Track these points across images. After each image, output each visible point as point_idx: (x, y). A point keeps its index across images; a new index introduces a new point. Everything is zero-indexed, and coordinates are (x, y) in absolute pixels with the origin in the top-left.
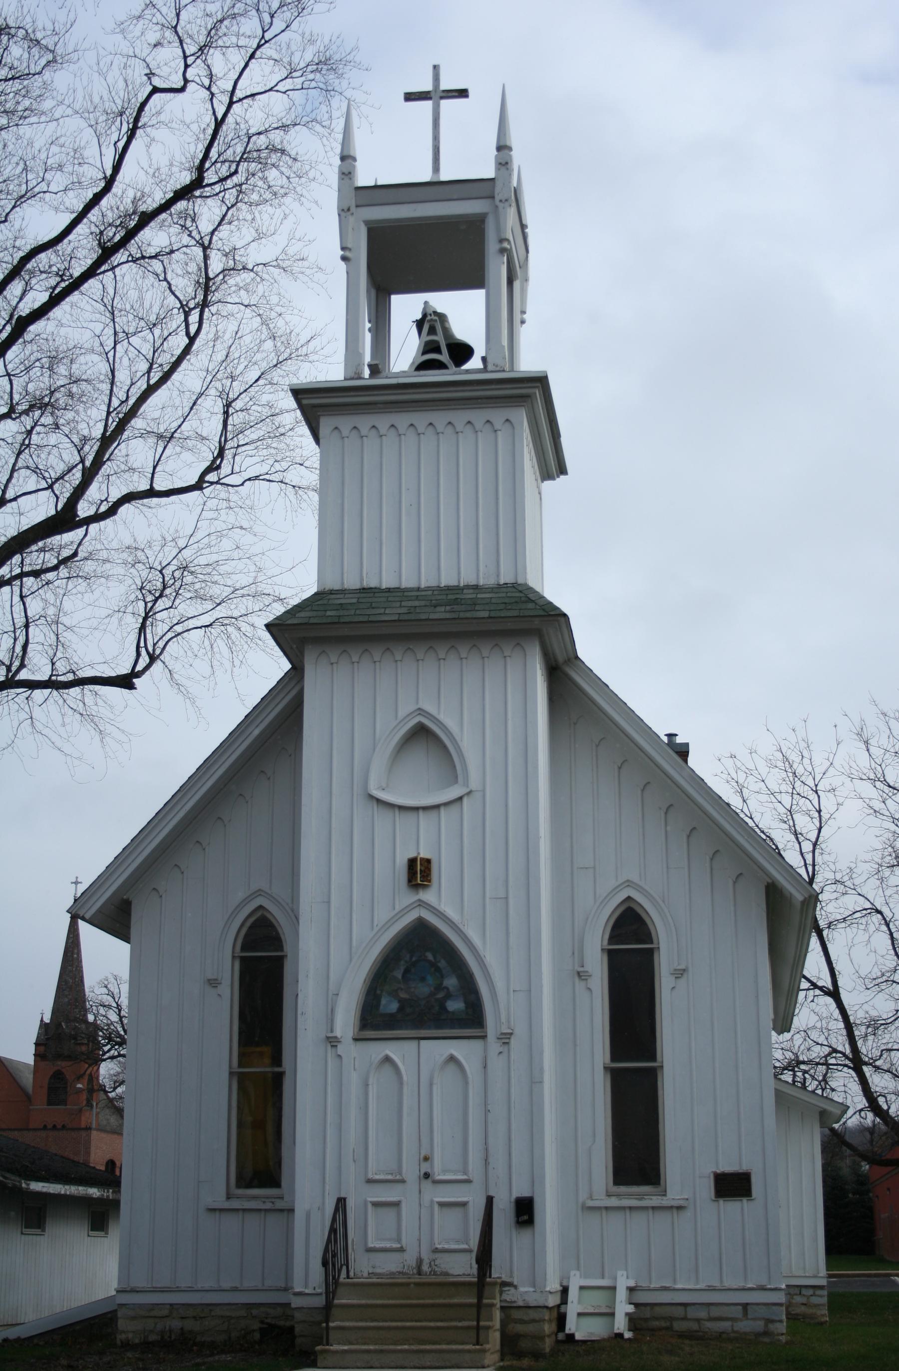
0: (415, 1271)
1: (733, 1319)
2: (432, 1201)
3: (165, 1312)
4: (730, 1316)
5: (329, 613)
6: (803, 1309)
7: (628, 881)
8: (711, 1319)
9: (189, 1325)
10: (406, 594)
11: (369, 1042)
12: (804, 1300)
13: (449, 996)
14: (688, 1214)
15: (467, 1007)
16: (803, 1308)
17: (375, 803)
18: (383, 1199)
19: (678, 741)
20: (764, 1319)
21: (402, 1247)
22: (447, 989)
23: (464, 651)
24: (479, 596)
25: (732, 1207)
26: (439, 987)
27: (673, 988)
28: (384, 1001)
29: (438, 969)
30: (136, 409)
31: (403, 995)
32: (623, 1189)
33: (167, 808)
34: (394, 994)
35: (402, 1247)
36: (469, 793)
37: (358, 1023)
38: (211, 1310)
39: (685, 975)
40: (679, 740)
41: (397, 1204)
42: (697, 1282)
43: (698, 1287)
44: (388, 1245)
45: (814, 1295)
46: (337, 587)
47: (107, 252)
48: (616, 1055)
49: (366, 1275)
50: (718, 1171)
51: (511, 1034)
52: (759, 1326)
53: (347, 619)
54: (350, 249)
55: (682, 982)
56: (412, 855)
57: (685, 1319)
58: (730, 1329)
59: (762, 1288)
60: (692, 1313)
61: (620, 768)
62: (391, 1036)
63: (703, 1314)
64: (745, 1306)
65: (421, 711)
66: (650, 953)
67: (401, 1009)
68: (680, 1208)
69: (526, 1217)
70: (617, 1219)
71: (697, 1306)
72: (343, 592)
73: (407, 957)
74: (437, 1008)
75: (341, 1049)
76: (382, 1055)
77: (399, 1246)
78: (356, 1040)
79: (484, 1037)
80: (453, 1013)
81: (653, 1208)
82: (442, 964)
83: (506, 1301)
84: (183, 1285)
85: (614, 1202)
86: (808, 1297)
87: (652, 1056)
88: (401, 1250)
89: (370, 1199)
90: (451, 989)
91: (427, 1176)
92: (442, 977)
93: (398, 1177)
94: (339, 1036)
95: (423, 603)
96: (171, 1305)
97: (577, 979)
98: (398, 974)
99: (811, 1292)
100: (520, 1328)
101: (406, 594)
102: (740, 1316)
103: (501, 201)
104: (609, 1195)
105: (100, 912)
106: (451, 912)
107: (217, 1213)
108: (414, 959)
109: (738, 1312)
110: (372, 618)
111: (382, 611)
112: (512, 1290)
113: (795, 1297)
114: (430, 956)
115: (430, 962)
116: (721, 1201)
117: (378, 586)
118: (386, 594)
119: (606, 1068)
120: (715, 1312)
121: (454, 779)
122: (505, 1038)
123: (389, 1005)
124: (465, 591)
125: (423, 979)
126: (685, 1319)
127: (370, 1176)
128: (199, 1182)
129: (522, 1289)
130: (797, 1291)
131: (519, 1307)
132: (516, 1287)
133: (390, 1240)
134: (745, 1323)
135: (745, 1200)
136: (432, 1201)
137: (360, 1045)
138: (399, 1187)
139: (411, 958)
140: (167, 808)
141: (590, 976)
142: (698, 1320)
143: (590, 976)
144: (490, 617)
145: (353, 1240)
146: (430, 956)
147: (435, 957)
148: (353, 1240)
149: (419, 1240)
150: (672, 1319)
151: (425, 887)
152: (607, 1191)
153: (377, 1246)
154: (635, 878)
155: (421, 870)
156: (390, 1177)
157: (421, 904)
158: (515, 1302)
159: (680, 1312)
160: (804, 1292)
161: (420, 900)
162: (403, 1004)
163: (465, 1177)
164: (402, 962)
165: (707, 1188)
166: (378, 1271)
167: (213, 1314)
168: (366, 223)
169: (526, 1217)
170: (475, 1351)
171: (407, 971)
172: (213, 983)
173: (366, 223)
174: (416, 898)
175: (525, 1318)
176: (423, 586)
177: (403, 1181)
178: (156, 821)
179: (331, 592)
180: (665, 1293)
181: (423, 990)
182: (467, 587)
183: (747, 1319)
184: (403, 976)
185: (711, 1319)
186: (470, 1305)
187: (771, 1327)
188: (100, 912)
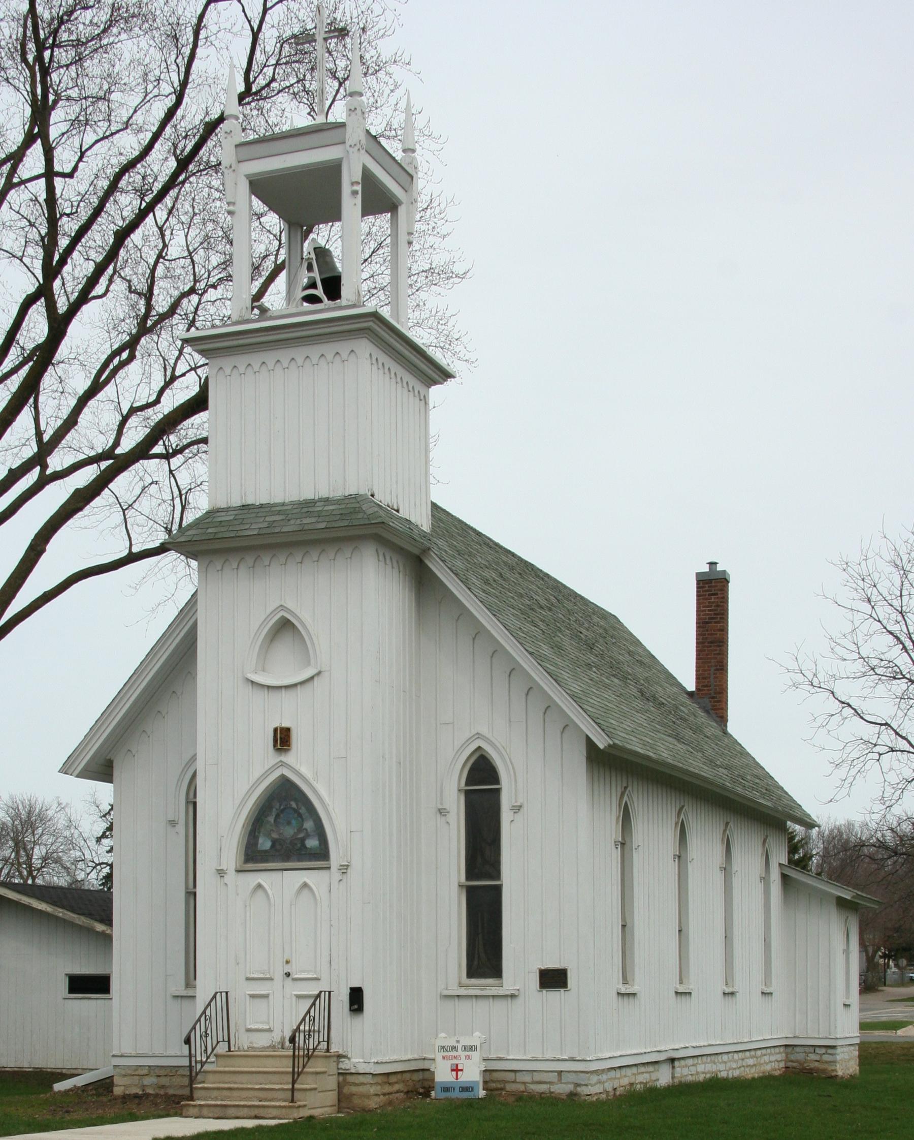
0: (280, 1046)
1: (550, 1083)
2: (291, 994)
3: (145, 1072)
4: (549, 1080)
5: (210, 530)
6: (817, 1064)
7: (478, 733)
8: (534, 1083)
9: (164, 1081)
10: (273, 509)
11: (247, 873)
12: (818, 1058)
13: (308, 836)
14: (519, 1001)
15: (320, 844)
16: (817, 1064)
17: (250, 684)
18: (258, 992)
19: (718, 569)
20: (573, 1083)
21: (270, 1028)
22: (306, 830)
23: (315, 554)
24: (326, 508)
25: (554, 996)
26: (300, 829)
27: (512, 821)
28: (261, 840)
29: (300, 815)
30: (327, 263)
31: (275, 836)
32: (474, 981)
33: (126, 688)
34: (268, 835)
35: (270, 1028)
36: (319, 673)
37: (243, 858)
38: (177, 1071)
39: (522, 810)
40: (719, 568)
41: (266, 996)
42: (525, 1053)
43: (524, 1058)
44: (260, 1026)
45: (826, 1053)
46: (224, 505)
47: (183, 164)
48: (470, 875)
49: (246, 1048)
50: (543, 968)
51: (348, 866)
52: (569, 1088)
53: (220, 536)
54: (234, 204)
55: (519, 817)
56: (277, 725)
57: (514, 1082)
58: (548, 1091)
59: (573, 1060)
60: (520, 1077)
61: (474, 639)
62: (263, 868)
63: (527, 1078)
64: (560, 1073)
65: (282, 607)
66: (498, 791)
67: (273, 846)
68: (513, 996)
69: (356, 1007)
70: (465, 1005)
71: (524, 1073)
72: (227, 510)
73: (278, 806)
74: (299, 845)
75: (227, 879)
76: (256, 883)
77: (268, 1027)
78: (238, 871)
79: (329, 868)
80: (311, 849)
81: (493, 996)
82: (303, 810)
83: (341, 1069)
84: (157, 1053)
85: (463, 992)
86: (821, 1055)
87: (497, 875)
88: (270, 1030)
89: (248, 993)
90: (309, 830)
91: (288, 975)
92: (303, 820)
93: (268, 976)
94: (225, 869)
95: (281, 517)
96: (149, 1066)
97: (438, 815)
98: (271, 819)
99: (823, 1051)
100: (354, 1089)
101: (273, 509)
102: (555, 1080)
103: (351, 146)
104: (461, 985)
105: (86, 770)
106: (304, 770)
107: (179, 999)
108: (282, 807)
109: (553, 1077)
110: (241, 534)
111: (247, 527)
112: (347, 1061)
113: (810, 1055)
114: (294, 805)
115: (294, 809)
116: (544, 991)
117: (254, 503)
118: (257, 510)
119: (461, 886)
120: (537, 1077)
121: (307, 663)
122: (344, 869)
123: (265, 844)
124: (318, 504)
125: (289, 823)
126: (514, 1082)
127: (249, 975)
128: (166, 976)
129: (353, 1060)
130: (812, 1050)
131: (352, 1074)
132: (349, 1059)
133: (262, 1023)
134: (560, 1085)
135: (562, 990)
136: (291, 994)
137: (241, 875)
138: (268, 983)
139: (280, 805)
140: (126, 688)
141: (448, 812)
142: (524, 1083)
143: (448, 812)
144: (326, 528)
145: (236, 1024)
146: (294, 805)
147: (297, 805)
148: (236, 1024)
149: (283, 1023)
150: (505, 1082)
151: (287, 751)
152: (460, 983)
153: (253, 1027)
154: (484, 731)
155: (281, 738)
156: (262, 976)
157: (283, 764)
158: (348, 1070)
159: (511, 1076)
160: (818, 1050)
161: (281, 761)
162: (274, 842)
163: (315, 976)
164: (274, 810)
165: (535, 979)
166: (255, 1045)
167: (178, 1073)
168: (247, 176)
169: (356, 1007)
170: (290, 1107)
171: (277, 816)
172: (173, 823)
173: (247, 176)
174: (278, 760)
175: (357, 1082)
176: (287, 501)
177: (271, 979)
178: (119, 698)
179: (219, 510)
180: (501, 1062)
181: (289, 832)
182: (320, 500)
183: (561, 1083)
184: (275, 821)
185: (534, 1083)
186: (287, 1073)
187: (579, 1089)
188: (86, 770)
